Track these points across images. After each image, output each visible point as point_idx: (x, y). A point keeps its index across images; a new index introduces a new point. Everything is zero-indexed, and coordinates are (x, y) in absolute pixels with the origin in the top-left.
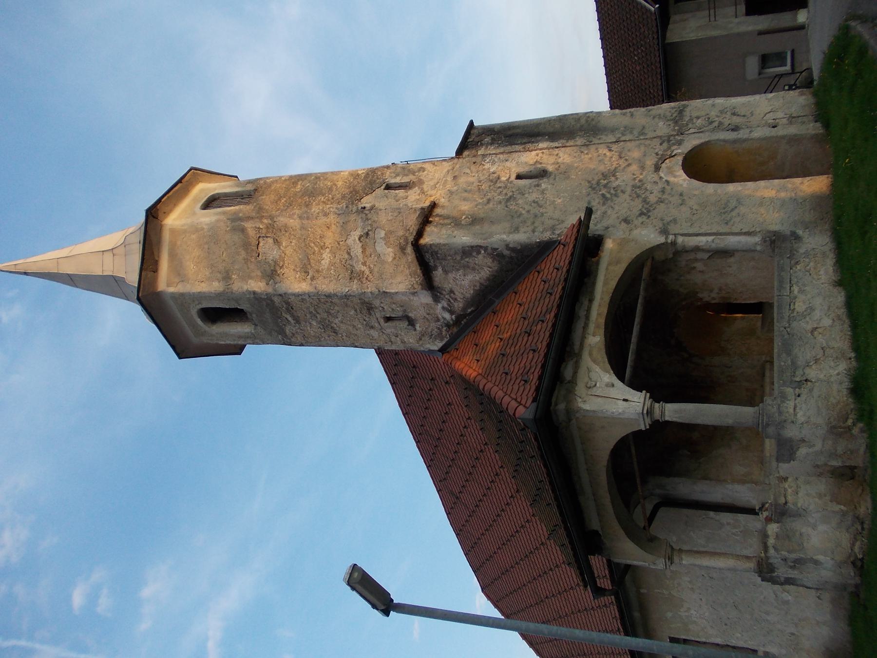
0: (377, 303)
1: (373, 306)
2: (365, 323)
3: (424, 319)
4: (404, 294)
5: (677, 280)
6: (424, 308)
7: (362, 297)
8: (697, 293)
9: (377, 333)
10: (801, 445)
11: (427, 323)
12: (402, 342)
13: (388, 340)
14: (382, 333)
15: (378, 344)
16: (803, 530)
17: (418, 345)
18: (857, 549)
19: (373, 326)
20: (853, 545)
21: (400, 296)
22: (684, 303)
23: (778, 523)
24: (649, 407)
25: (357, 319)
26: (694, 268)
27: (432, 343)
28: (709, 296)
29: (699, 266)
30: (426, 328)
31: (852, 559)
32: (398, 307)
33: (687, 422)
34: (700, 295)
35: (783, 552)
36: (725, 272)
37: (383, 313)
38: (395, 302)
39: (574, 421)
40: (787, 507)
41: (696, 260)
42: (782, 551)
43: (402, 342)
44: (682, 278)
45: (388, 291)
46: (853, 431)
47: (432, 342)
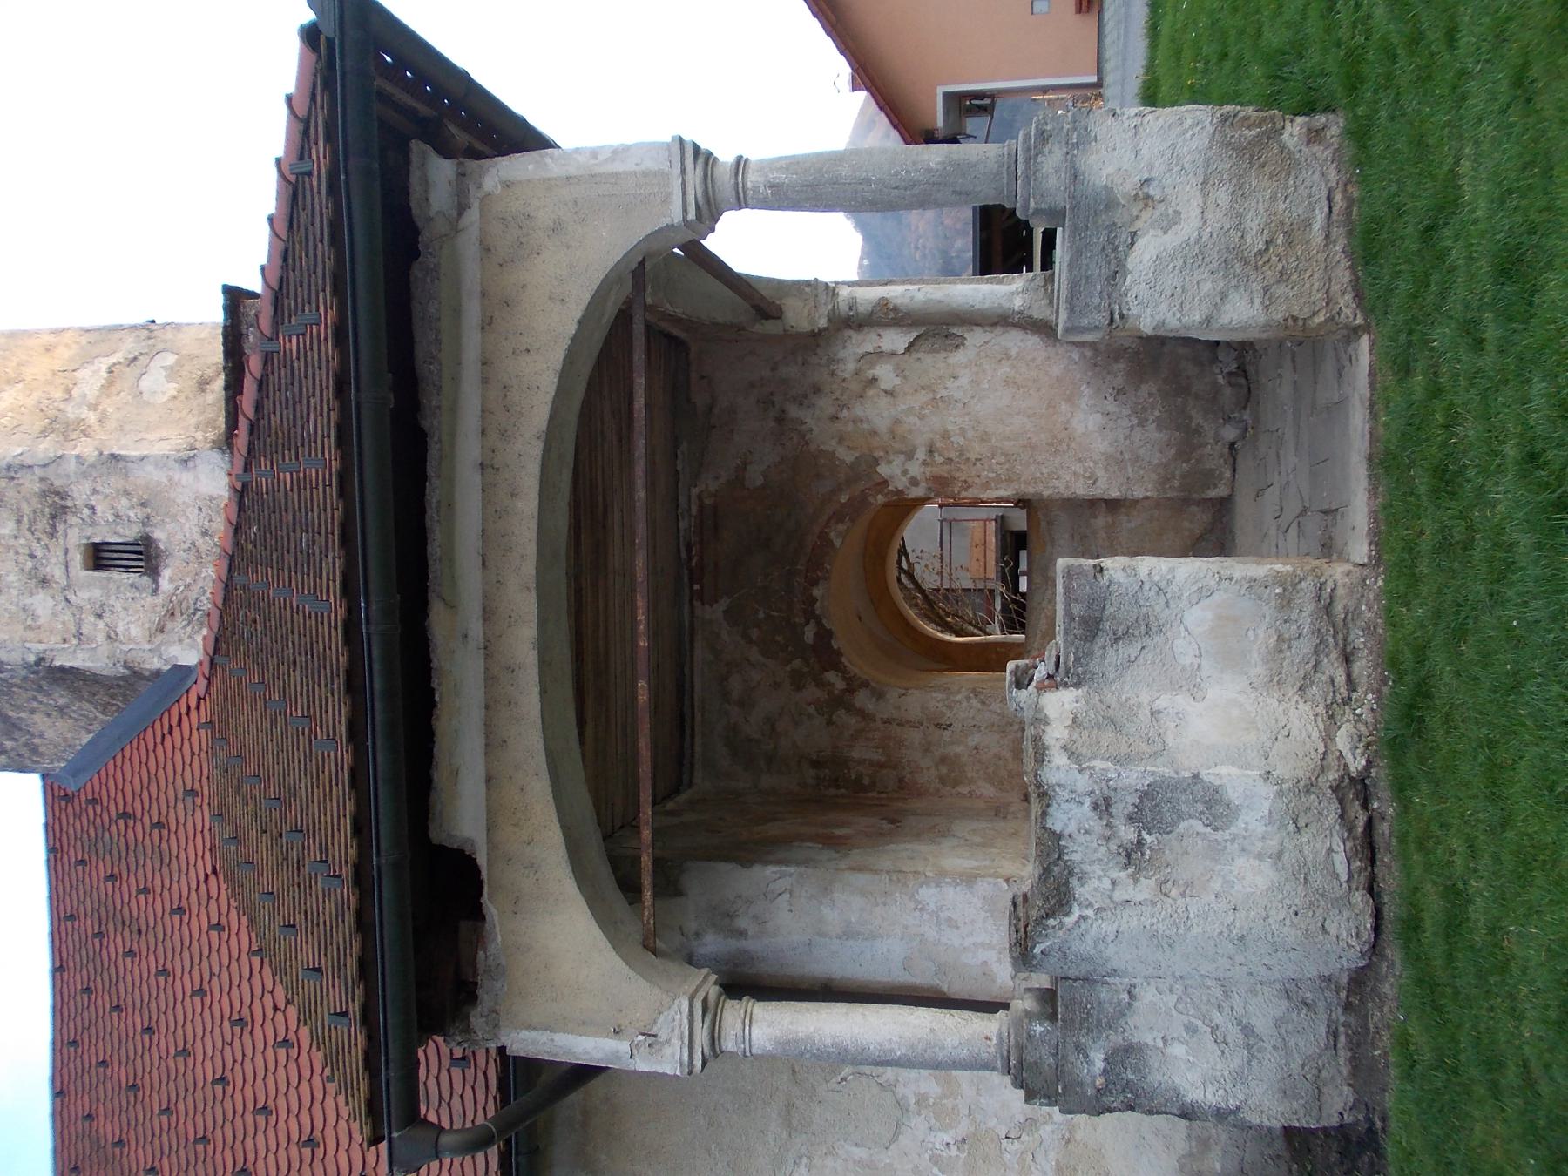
0: (81, 493)
1: (69, 503)
2: (30, 564)
3: (189, 549)
4: (161, 462)
5: (834, 418)
6: (200, 509)
7: (50, 473)
8: (876, 462)
9: (51, 602)
10: (1139, 224)
11: (194, 566)
12: (109, 637)
13: (74, 630)
14: (64, 603)
15: (41, 647)
16: (1162, 703)
17: (148, 647)
18: (1343, 741)
19: (49, 577)
20: (1328, 738)
21: (150, 468)
22: (844, 498)
23: (1077, 685)
24: (700, 199)
25: (12, 553)
26: (875, 379)
27: (187, 641)
28: (905, 472)
29: (885, 373)
30: (187, 586)
31: (1333, 776)
32: (132, 507)
33: (839, 1004)
34: (883, 470)
35: (1098, 764)
36: (944, 393)
37: (89, 531)
38: (130, 488)
39: (472, 216)
40: (1104, 580)
41: (879, 355)
42: (1093, 758)
43: (109, 637)
44: (845, 413)
45: (122, 453)
46: (1286, 136)
47: (190, 637)
